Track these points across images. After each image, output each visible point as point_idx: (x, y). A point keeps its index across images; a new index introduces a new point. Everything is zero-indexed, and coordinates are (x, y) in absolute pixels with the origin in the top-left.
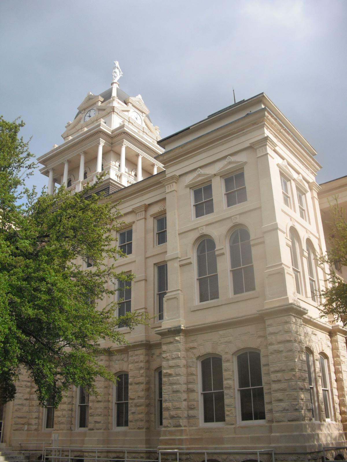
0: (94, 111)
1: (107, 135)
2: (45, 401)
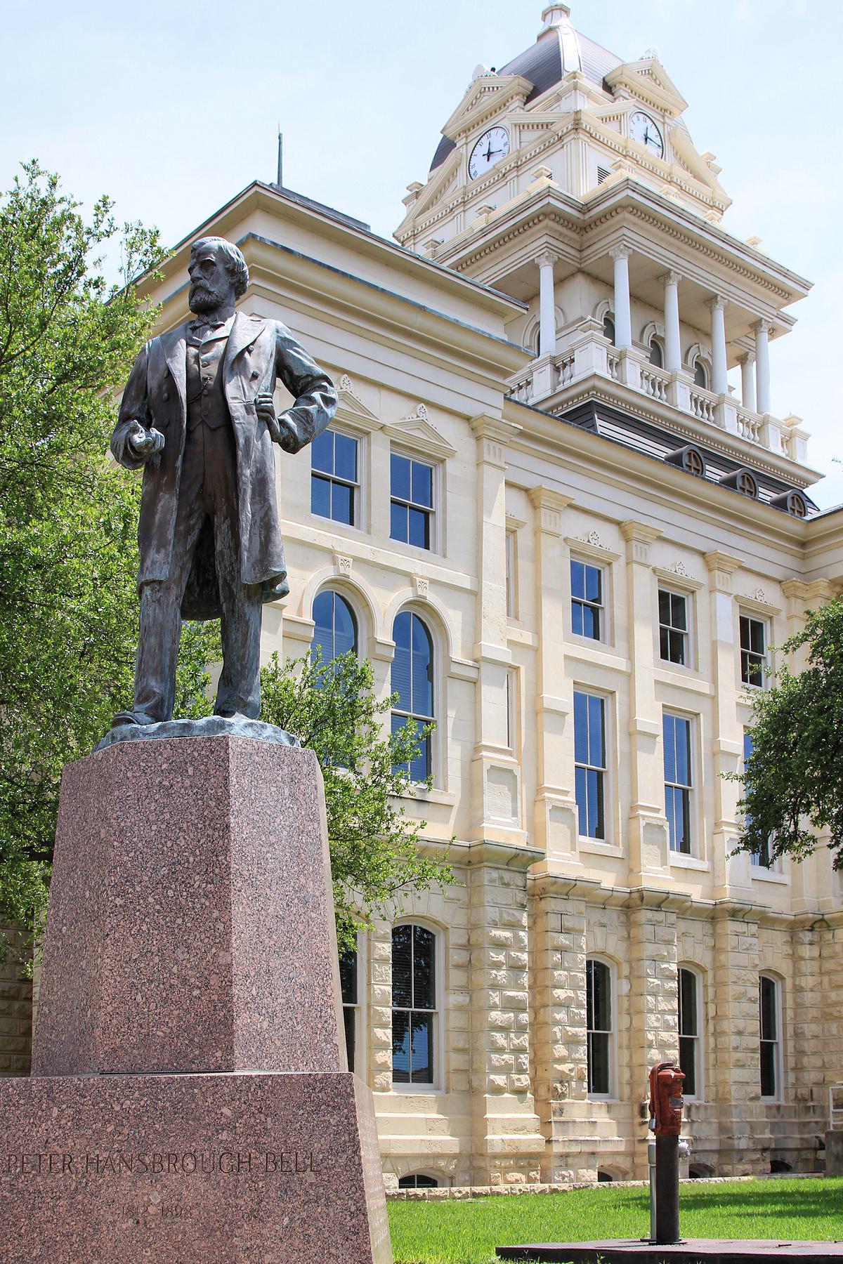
0: (501, 132)
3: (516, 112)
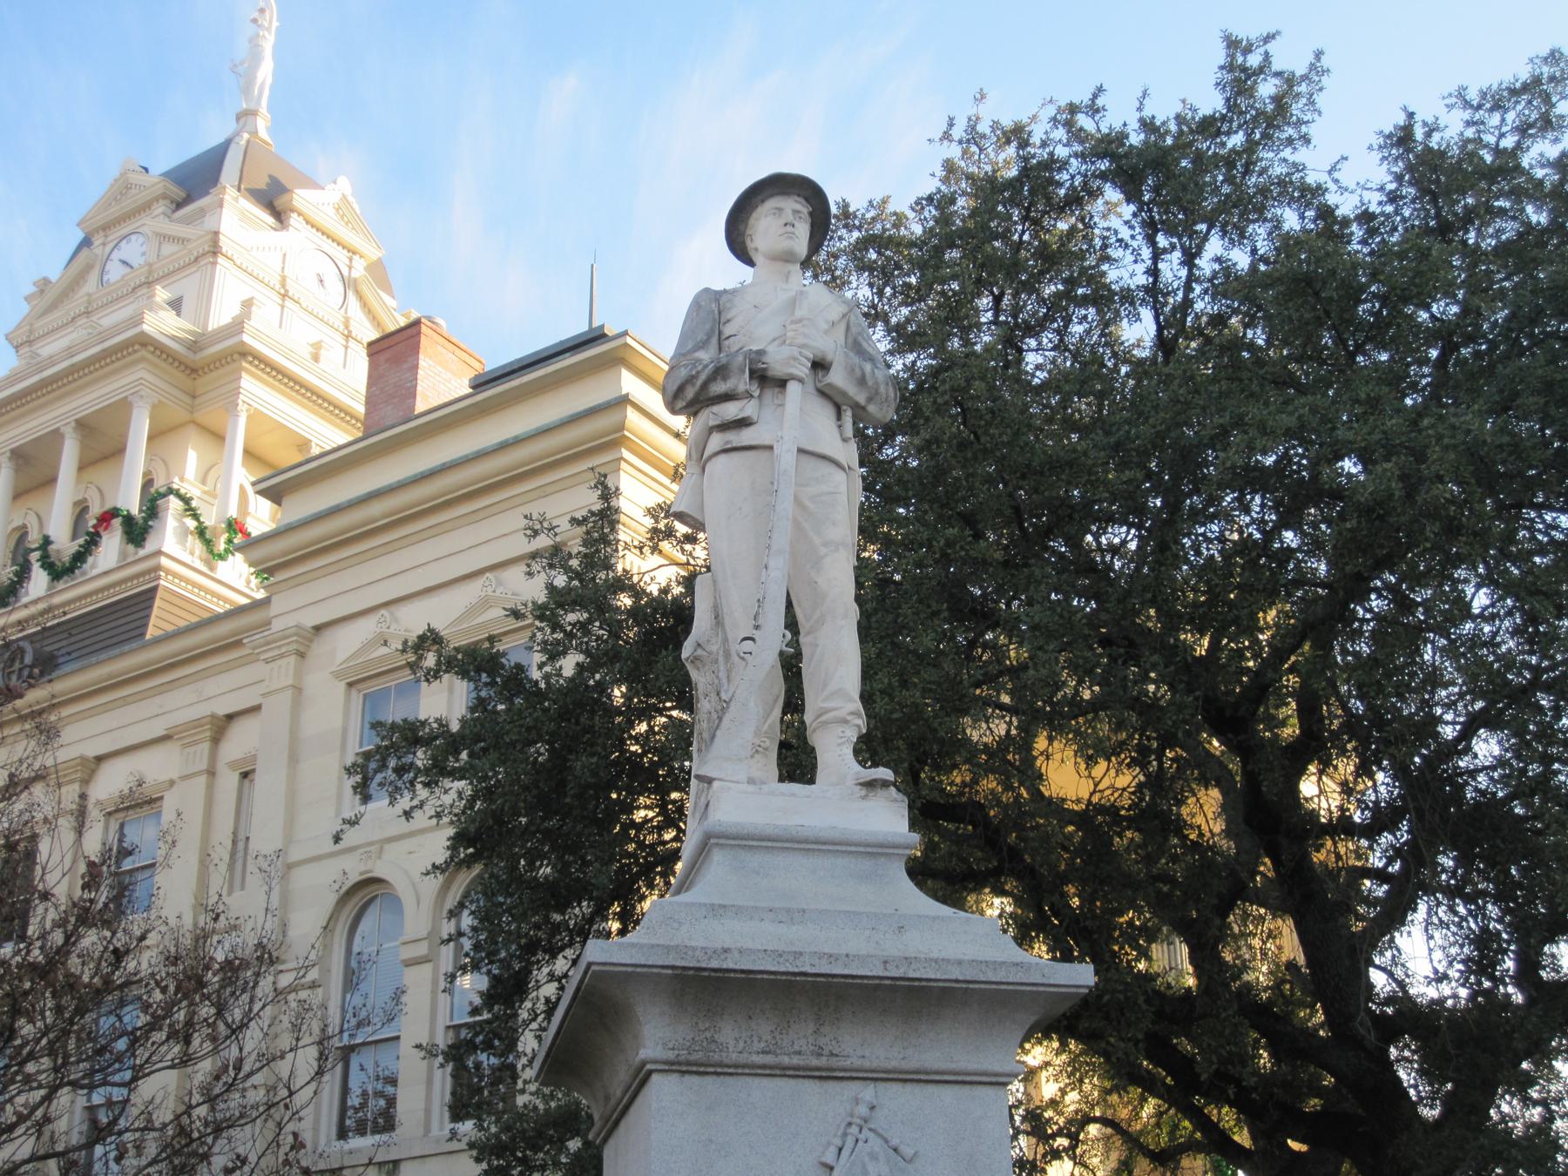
0: (141, 239)
1: (180, 363)
2: (901, 362)
3: (157, 221)
